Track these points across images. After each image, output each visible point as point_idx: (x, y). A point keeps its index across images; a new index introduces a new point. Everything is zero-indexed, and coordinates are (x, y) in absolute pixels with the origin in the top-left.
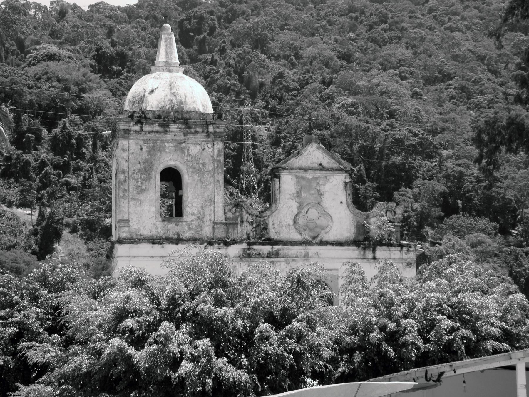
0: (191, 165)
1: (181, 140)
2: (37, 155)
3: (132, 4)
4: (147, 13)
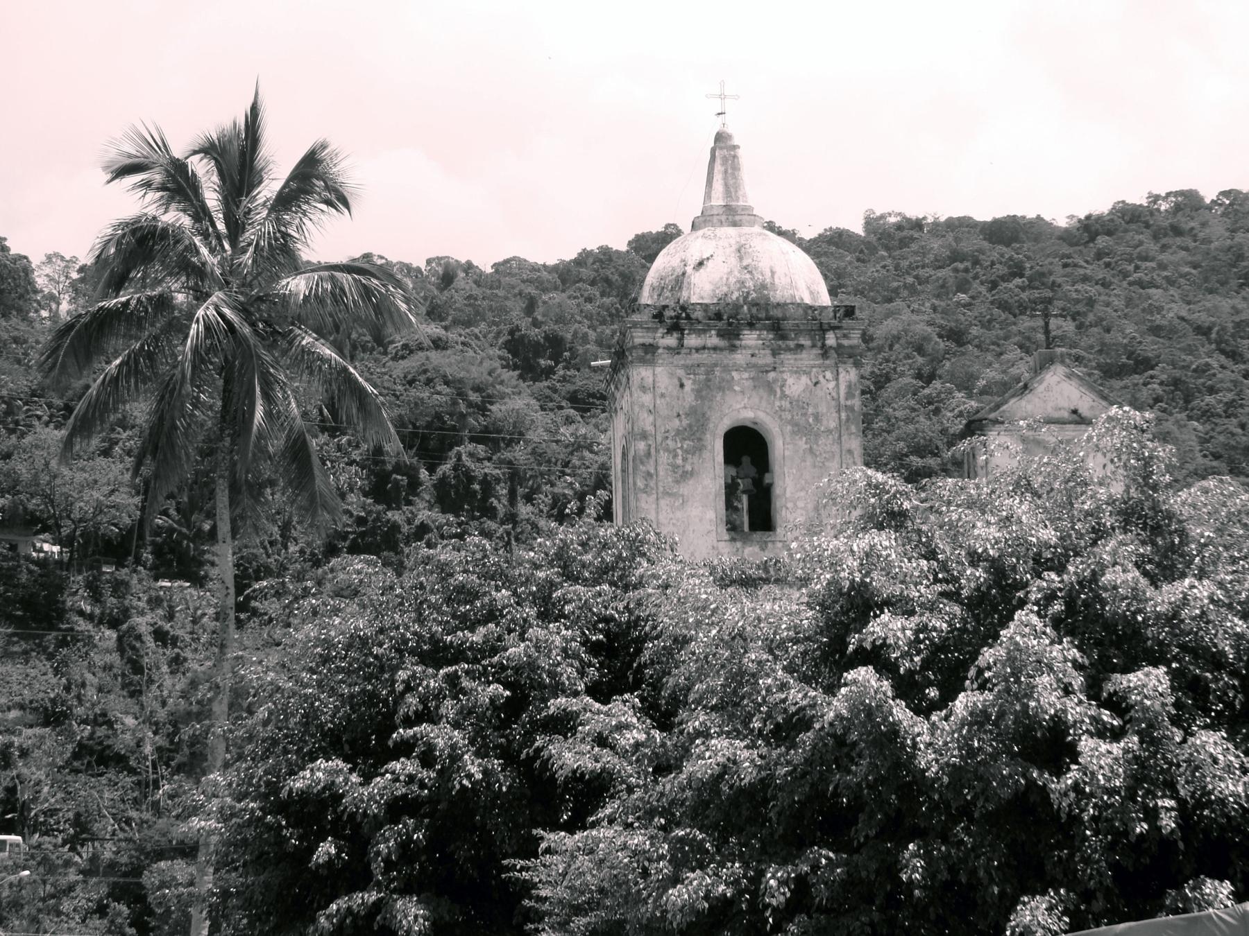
0: (789, 417)
1: (767, 365)
2: (412, 512)
3: (568, 259)
4: (593, 274)
